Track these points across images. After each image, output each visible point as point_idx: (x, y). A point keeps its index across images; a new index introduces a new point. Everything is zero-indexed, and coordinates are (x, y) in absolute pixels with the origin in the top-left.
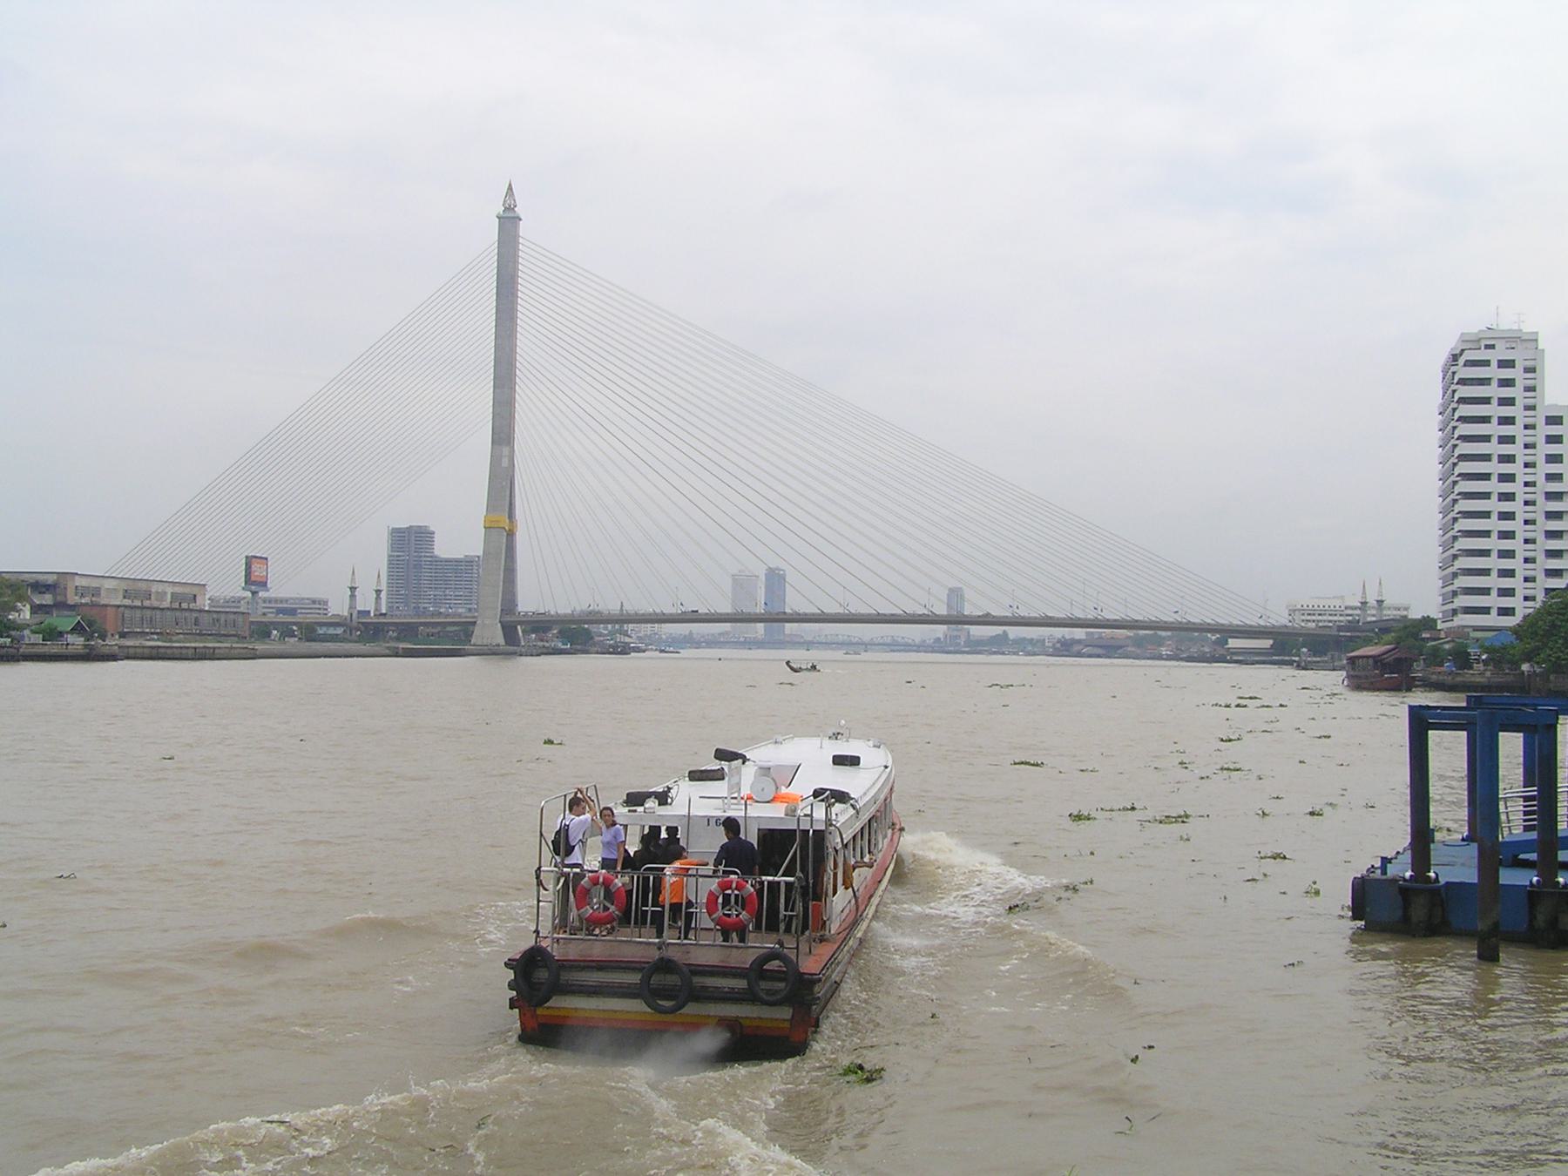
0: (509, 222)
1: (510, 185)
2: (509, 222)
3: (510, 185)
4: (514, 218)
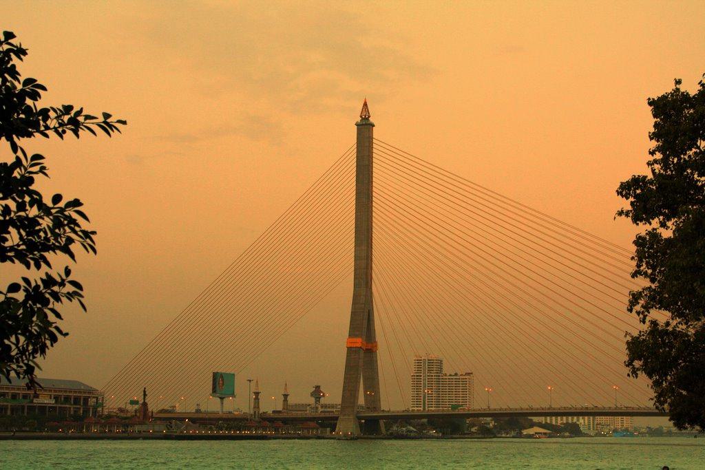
0: (365, 127)
1: (365, 104)
2: (365, 127)
3: (365, 104)
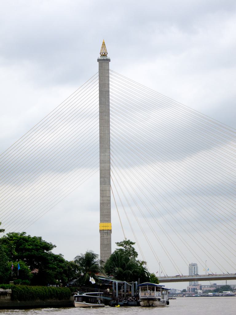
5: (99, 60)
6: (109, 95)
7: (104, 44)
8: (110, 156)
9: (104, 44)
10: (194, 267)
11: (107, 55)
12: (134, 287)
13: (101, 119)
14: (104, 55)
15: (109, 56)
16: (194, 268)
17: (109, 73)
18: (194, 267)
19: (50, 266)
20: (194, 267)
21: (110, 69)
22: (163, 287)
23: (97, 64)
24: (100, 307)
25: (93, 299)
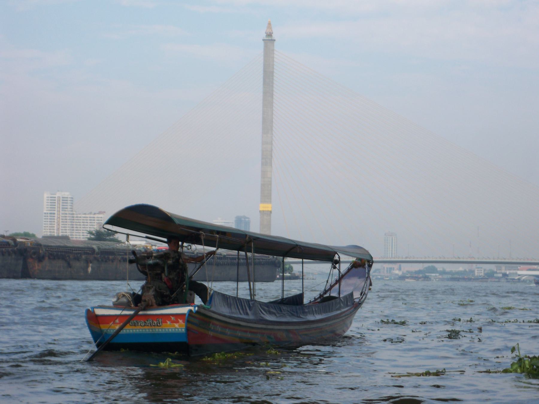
4: (272, 40)
5: (264, 40)
6: (273, 76)
7: (269, 24)
8: (272, 137)
9: (269, 24)
10: (391, 237)
11: (272, 35)
12: (258, 250)
13: (264, 99)
14: (270, 35)
15: (274, 36)
16: (391, 239)
17: (274, 53)
18: (392, 238)
19: (257, 262)
20: (392, 238)
21: (275, 49)
22: (63, 287)
23: (262, 42)
24: (34, 382)
25: (391, 256)
